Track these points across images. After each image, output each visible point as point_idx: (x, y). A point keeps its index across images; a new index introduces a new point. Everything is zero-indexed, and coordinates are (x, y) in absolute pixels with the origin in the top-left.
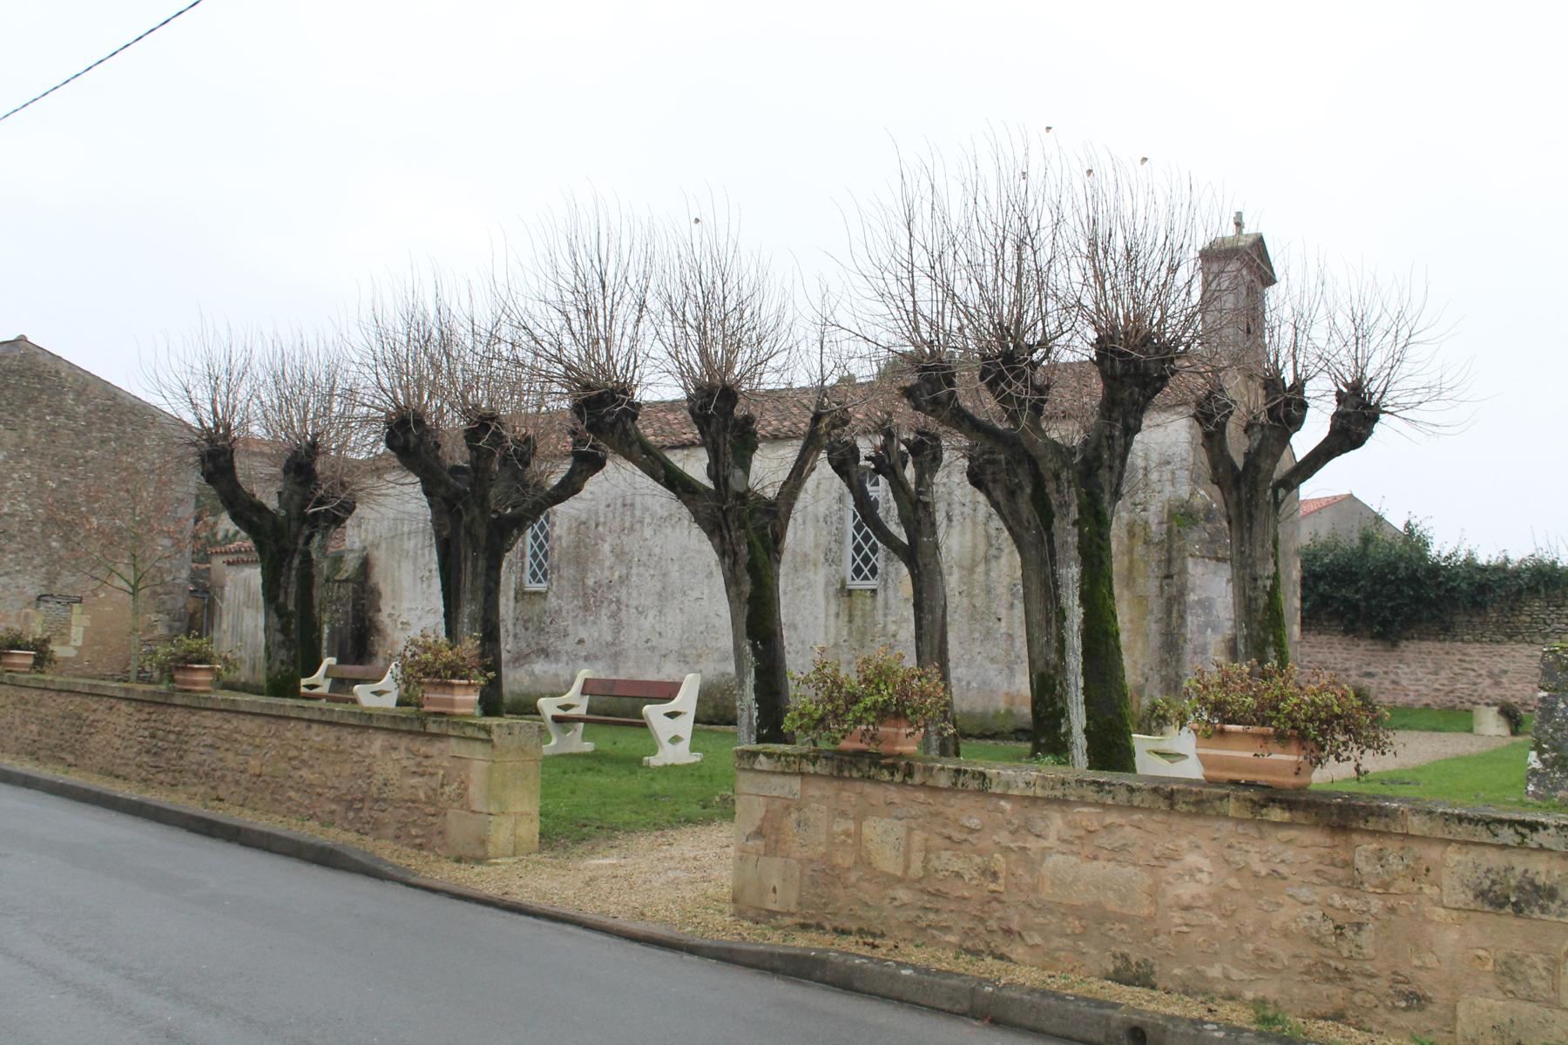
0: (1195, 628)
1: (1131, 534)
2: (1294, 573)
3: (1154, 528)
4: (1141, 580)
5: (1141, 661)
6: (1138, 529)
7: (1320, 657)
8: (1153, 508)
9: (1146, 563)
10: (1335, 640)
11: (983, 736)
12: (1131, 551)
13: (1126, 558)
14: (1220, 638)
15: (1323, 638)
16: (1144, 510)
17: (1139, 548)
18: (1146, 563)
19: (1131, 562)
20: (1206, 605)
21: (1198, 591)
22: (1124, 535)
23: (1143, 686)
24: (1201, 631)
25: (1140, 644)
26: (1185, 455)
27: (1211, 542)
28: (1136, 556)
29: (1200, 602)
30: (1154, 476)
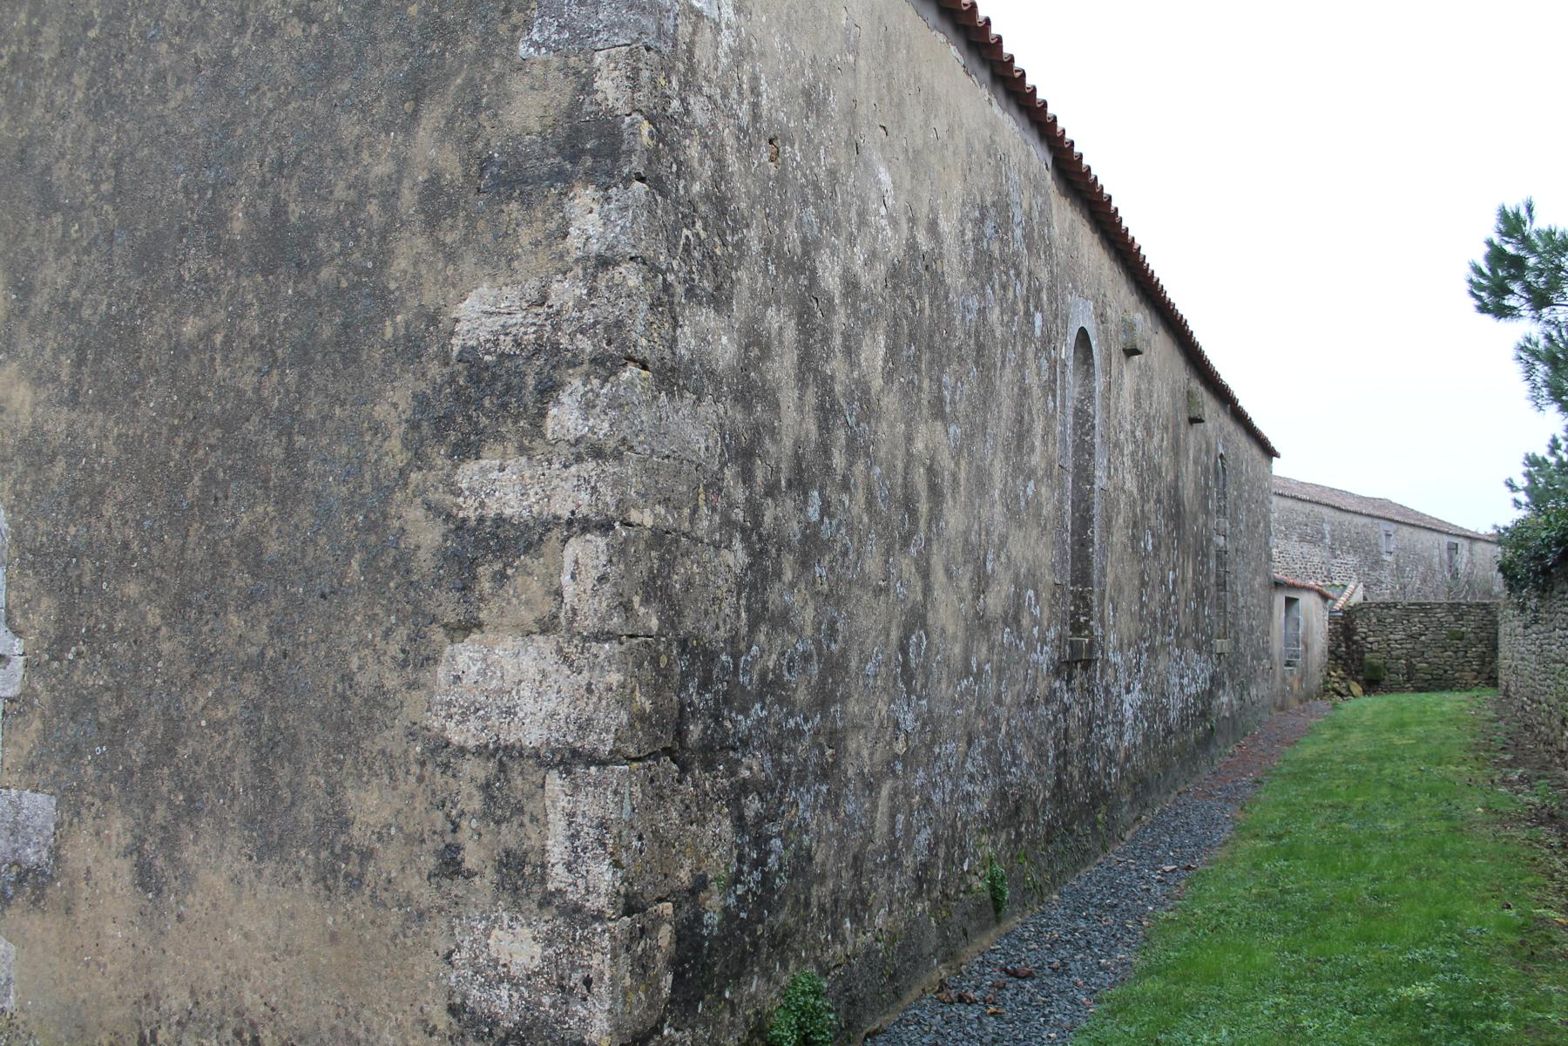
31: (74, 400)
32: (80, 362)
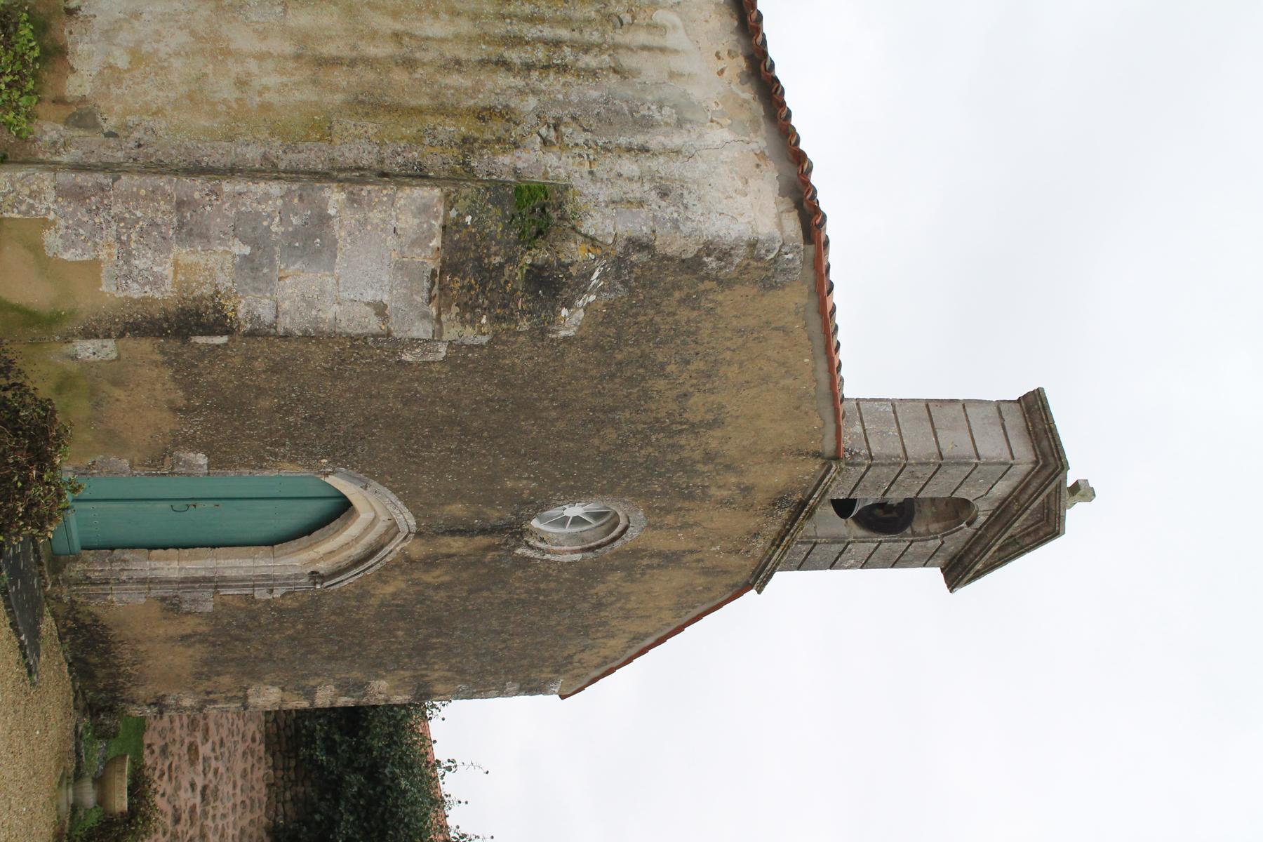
0: (248, 205)
1: (484, 115)
2: (384, 690)
3: (505, 160)
4: (371, 129)
5: (161, 125)
6: (497, 127)
7: (226, 789)
8: (551, 159)
9: (418, 140)
10: (259, 813)
11: (177, 547)
12: (442, 110)
13: (424, 101)
14: (225, 281)
15: (261, 792)
16: (545, 142)
17: (450, 129)
18: (418, 140)
19: (419, 111)
20: (313, 240)
21: (350, 218)
22: (482, 100)
23: (96, 126)
24: (248, 227)
25: (204, 122)
26: (686, 228)
27: (480, 269)
28: (430, 121)
29: (323, 219)
30: (628, 166)
31: (382, 605)
32: (397, 606)
